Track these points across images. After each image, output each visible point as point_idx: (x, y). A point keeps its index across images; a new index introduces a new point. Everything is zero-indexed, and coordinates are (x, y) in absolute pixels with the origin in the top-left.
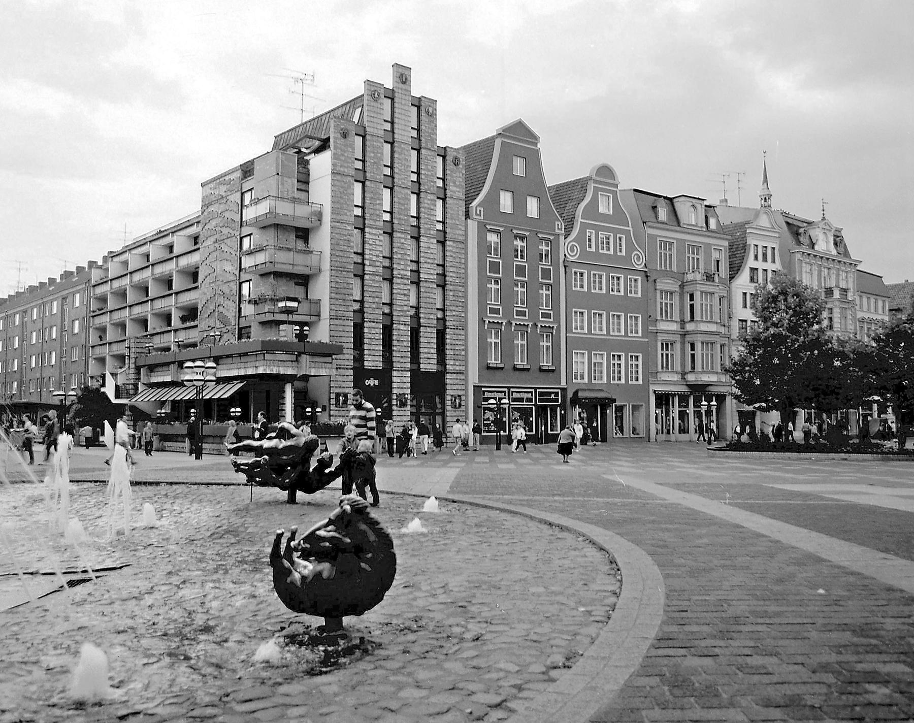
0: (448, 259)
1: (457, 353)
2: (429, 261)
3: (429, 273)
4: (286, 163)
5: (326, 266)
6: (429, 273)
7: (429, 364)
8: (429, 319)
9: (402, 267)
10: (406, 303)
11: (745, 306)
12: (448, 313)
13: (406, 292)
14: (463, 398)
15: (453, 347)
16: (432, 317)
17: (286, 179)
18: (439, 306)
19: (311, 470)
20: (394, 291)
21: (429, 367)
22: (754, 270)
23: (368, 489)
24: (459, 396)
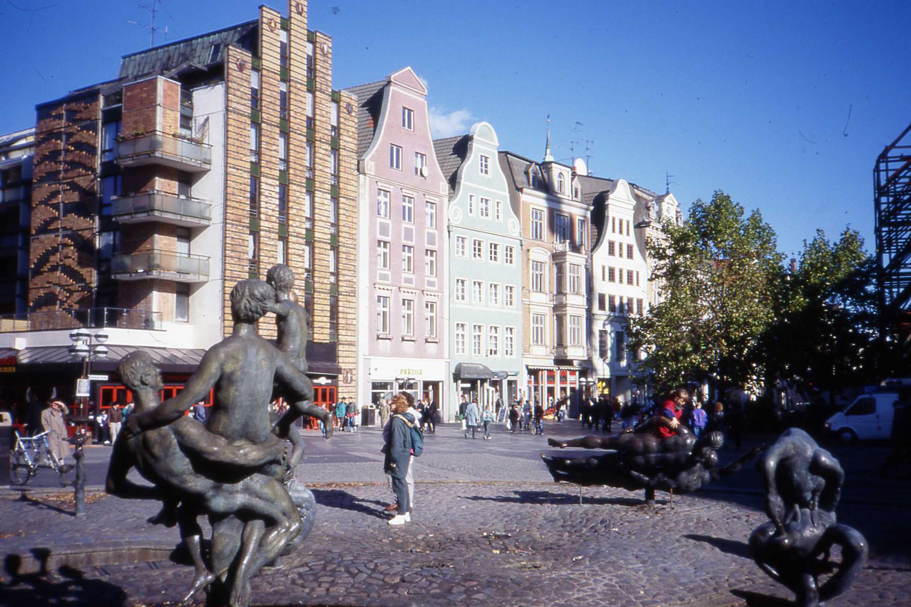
0: (342, 217)
1: (349, 322)
2: (323, 218)
3: (323, 233)
4: (169, 92)
5: (216, 214)
6: (323, 233)
7: (322, 335)
8: (323, 282)
9: (298, 224)
10: (300, 264)
11: (604, 279)
12: (341, 278)
13: (301, 252)
14: (354, 372)
15: (345, 316)
16: (325, 281)
17: (168, 112)
18: (332, 270)
19: (30, 587)
20: (290, 251)
21: (322, 337)
22: (611, 245)
23: (518, 496)
24: (351, 370)
